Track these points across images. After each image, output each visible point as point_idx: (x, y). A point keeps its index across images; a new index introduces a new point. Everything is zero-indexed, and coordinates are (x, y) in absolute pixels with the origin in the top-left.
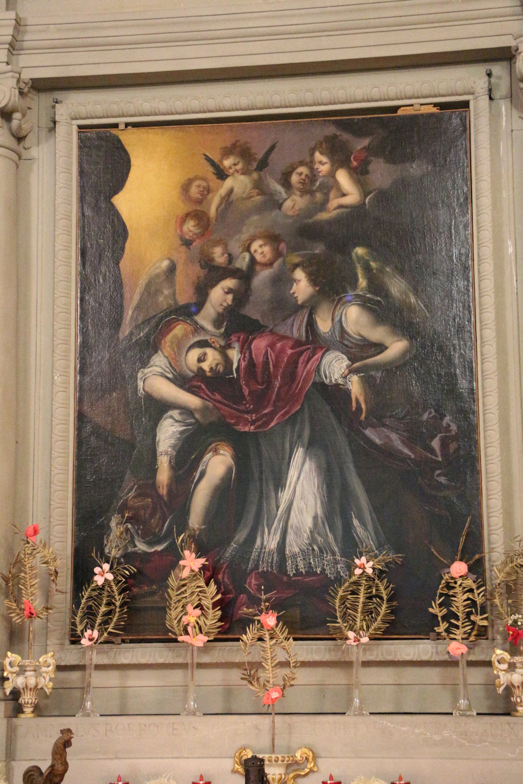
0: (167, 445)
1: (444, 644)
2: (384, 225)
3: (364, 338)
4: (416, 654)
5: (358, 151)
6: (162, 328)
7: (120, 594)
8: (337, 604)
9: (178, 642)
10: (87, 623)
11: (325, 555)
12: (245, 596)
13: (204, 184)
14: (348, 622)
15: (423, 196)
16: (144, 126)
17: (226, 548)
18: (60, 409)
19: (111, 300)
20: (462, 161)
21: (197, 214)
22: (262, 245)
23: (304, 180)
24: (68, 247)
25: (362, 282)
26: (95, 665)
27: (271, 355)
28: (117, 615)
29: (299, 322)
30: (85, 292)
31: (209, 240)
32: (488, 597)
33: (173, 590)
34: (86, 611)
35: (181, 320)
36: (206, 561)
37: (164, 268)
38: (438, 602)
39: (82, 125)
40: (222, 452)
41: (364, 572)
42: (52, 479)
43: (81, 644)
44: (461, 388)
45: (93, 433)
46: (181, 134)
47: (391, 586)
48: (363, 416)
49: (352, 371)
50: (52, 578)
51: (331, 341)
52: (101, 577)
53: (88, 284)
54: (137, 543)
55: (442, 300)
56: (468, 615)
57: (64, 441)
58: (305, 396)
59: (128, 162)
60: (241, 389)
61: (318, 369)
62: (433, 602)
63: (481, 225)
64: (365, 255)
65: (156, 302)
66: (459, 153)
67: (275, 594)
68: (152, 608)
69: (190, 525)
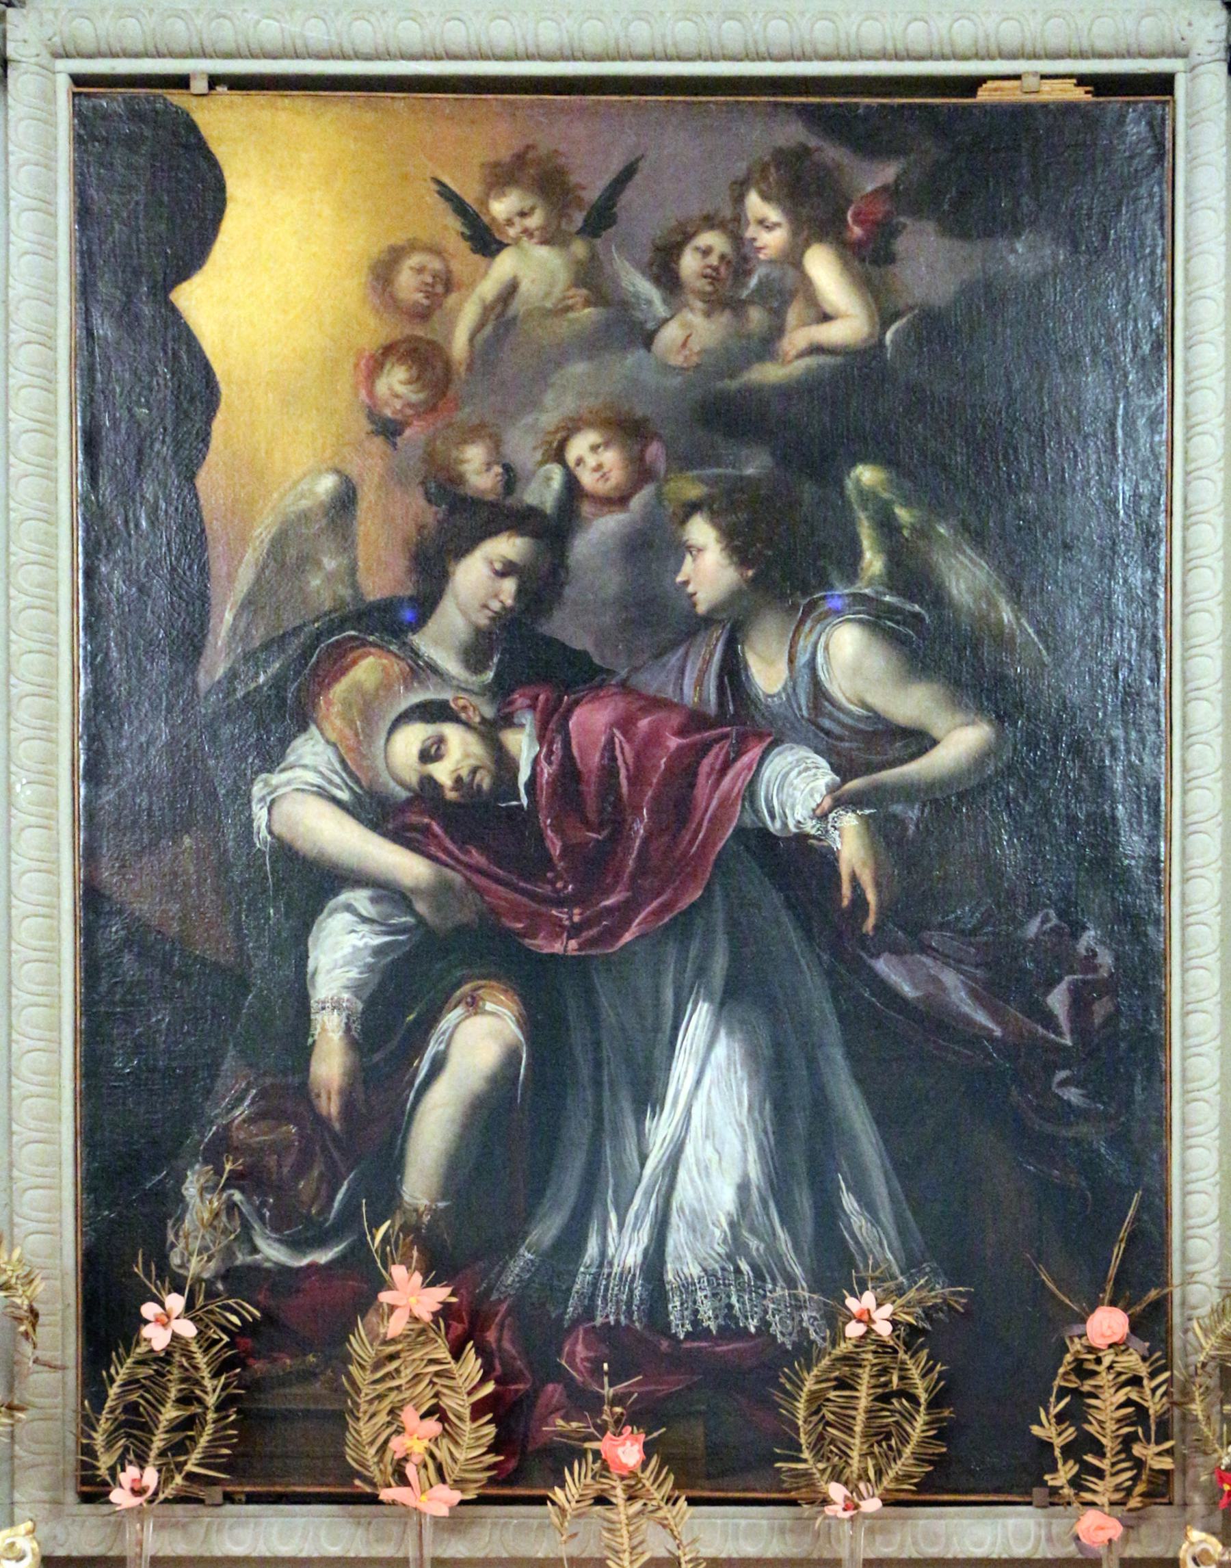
0: (339, 983)
1: (1066, 1517)
2: (933, 408)
3: (875, 713)
4: (999, 1541)
5: (867, 196)
6: (318, 662)
7: (216, 1375)
8: (801, 1414)
9: (381, 1503)
10: (126, 1449)
11: (770, 1286)
12: (560, 1387)
13: (436, 264)
14: (829, 1459)
15: (1042, 331)
16: (263, 88)
17: (506, 1263)
18: (33, 874)
19: (173, 579)
20: (1149, 241)
21: (415, 350)
22: (598, 446)
23: (716, 269)
24: (48, 424)
25: (873, 562)
26: (152, 1557)
27: (622, 748)
28: (209, 1428)
29: (699, 664)
30: (98, 552)
31: (450, 425)
32: (1176, 1397)
33: (362, 1367)
34: (123, 1417)
35: (373, 644)
36: (452, 1294)
37: (323, 497)
38: (1054, 1411)
39: (84, 75)
40: (489, 1006)
41: (870, 1331)
42: (14, 1063)
43: (109, 1502)
44: (1126, 856)
45: (127, 943)
46: (369, 117)
47: (938, 1368)
48: (871, 922)
49: (841, 801)
50: (22, 1328)
51: (786, 718)
52: (160, 1329)
53: (105, 531)
54: (260, 1242)
55: (1086, 620)
56: (1127, 1442)
57: (47, 962)
58: (717, 865)
59: (219, 188)
60: (541, 838)
61: (750, 793)
62: (1042, 1410)
63: (1194, 420)
64: (880, 489)
65: (301, 589)
66: (1144, 218)
67: (638, 1383)
68: (307, 1414)
69: (406, 1198)
